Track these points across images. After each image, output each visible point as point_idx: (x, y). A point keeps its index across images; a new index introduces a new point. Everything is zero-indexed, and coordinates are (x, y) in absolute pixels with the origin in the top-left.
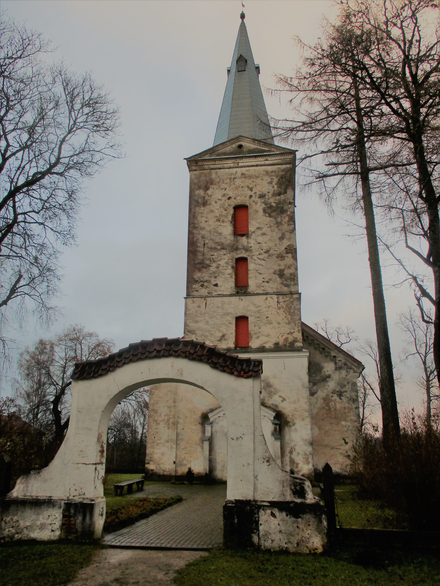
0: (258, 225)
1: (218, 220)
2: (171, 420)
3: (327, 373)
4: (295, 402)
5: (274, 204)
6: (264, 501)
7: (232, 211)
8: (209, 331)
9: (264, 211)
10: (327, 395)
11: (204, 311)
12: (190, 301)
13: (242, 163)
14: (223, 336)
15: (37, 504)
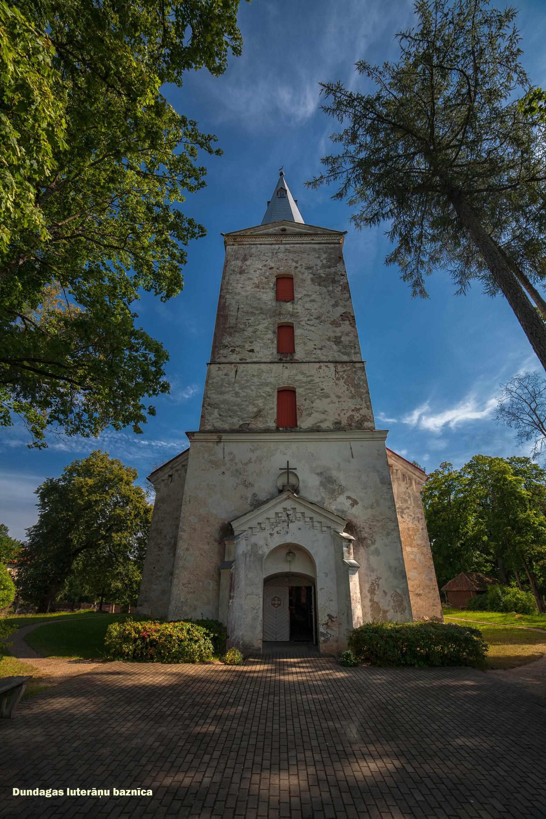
0: (305, 292)
1: (258, 287)
5: (323, 275)
7: (274, 280)
8: (239, 405)
9: (312, 280)
11: (233, 380)
12: (214, 367)
13: (285, 240)
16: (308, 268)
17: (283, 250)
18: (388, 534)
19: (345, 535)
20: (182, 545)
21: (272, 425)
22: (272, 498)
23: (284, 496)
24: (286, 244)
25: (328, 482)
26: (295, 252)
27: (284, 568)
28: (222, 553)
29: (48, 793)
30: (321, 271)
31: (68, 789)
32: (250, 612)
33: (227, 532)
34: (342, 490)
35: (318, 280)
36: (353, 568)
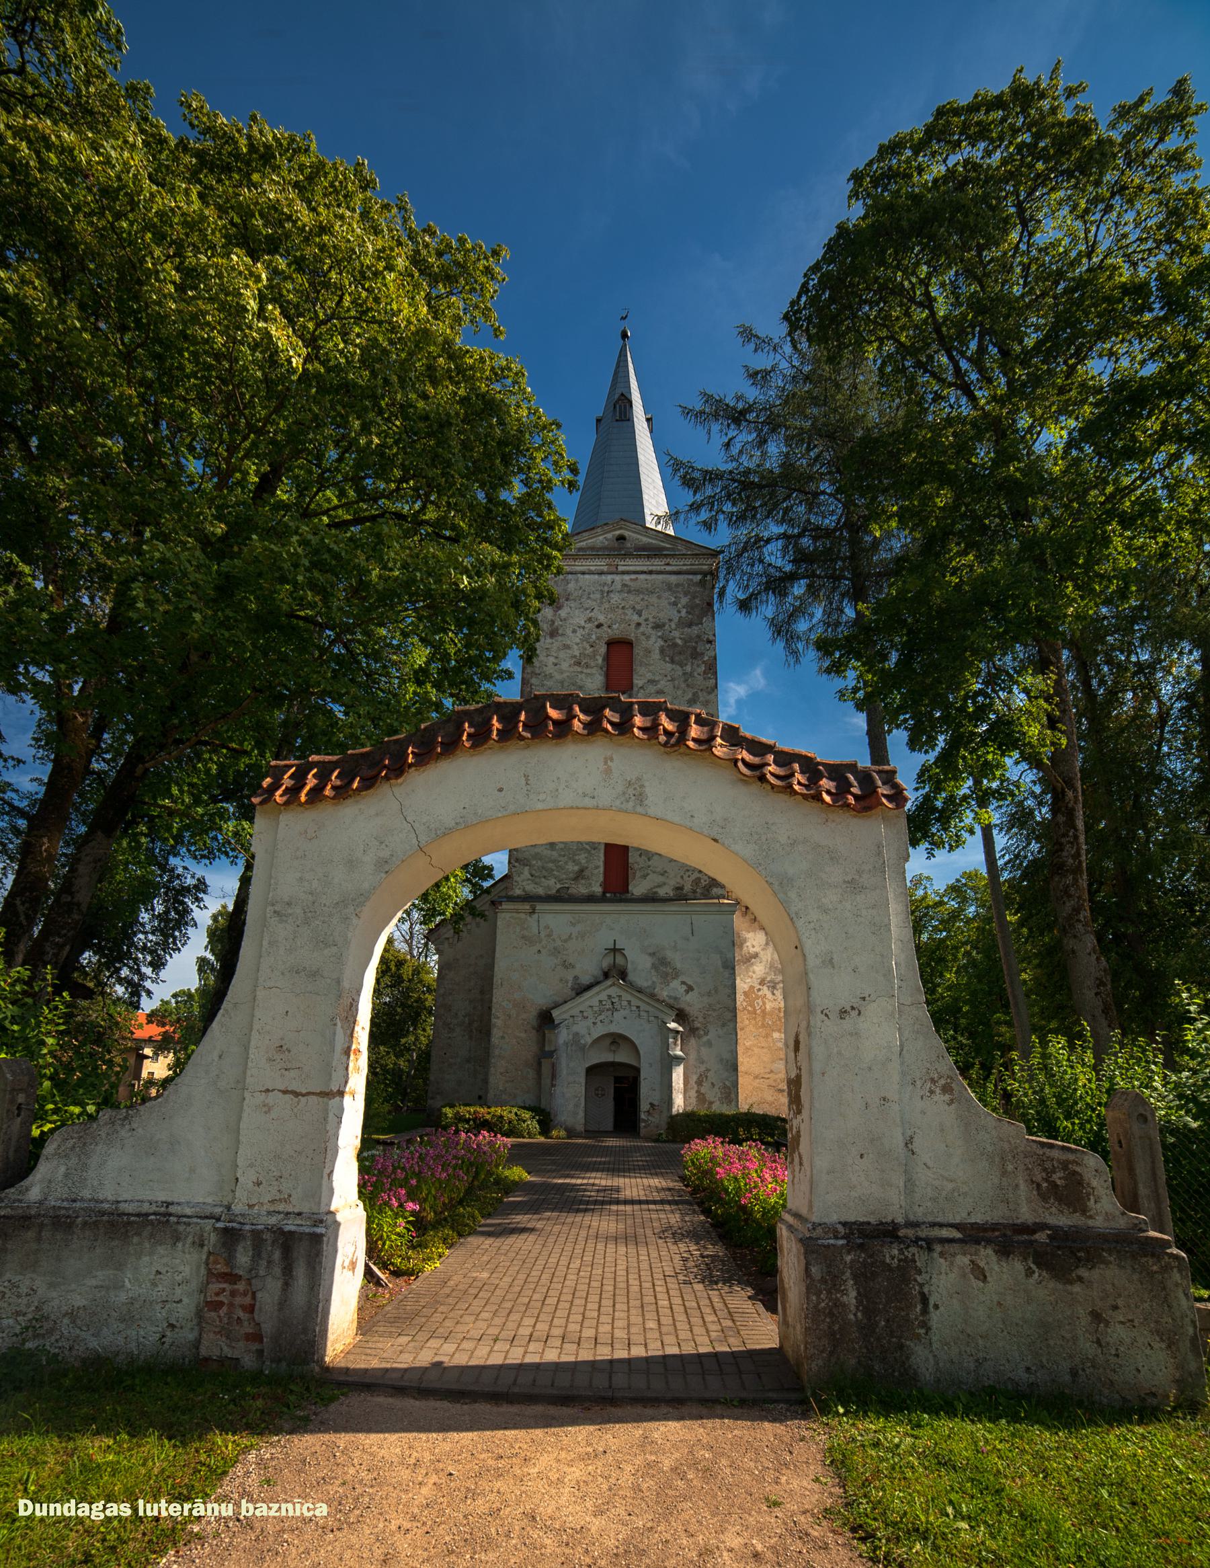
0: (649, 676)
1: (578, 664)
2: (475, 1025)
3: (752, 950)
4: (709, 994)
5: (679, 642)
6: (941, 1225)
7: (603, 649)
8: (554, 861)
9: (662, 651)
10: (752, 987)
13: (624, 565)
14: (582, 871)
15: (121, 1227)
16: (657, 626)
17: (619, 587)
18: (724, 1025)
19: (673, 1025)
20: (496, 1034)
21: (597, 889)
22: (598, 983)
23: (609, 982)
24: (623, 573)
25: (662, 965)
26: (638, 592)
27: (608, 1057)
28: (542, 1041)
29: (95, 1512)
30: (676, 634)
31: (141, 1502)
32: (571, 1097)
33: (546, 1020)
34: (676, 974)
35: (671, 652)
36: (679, 1060)
